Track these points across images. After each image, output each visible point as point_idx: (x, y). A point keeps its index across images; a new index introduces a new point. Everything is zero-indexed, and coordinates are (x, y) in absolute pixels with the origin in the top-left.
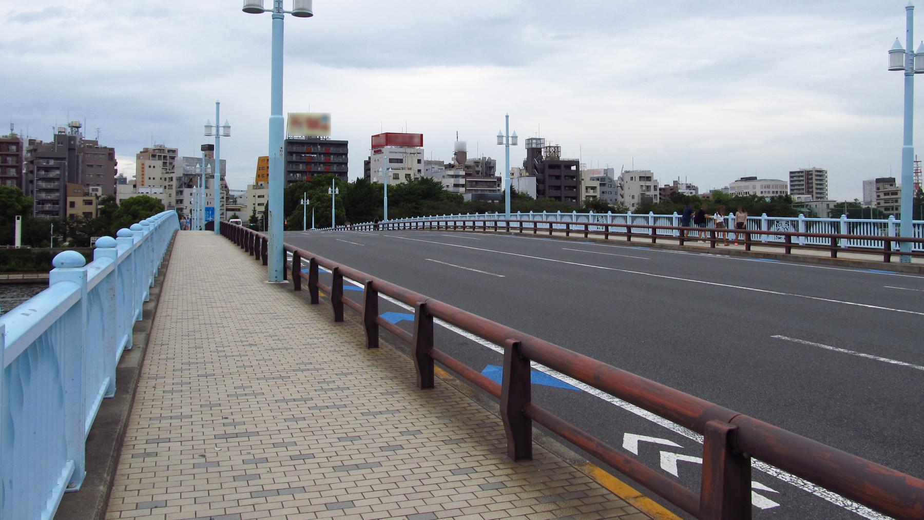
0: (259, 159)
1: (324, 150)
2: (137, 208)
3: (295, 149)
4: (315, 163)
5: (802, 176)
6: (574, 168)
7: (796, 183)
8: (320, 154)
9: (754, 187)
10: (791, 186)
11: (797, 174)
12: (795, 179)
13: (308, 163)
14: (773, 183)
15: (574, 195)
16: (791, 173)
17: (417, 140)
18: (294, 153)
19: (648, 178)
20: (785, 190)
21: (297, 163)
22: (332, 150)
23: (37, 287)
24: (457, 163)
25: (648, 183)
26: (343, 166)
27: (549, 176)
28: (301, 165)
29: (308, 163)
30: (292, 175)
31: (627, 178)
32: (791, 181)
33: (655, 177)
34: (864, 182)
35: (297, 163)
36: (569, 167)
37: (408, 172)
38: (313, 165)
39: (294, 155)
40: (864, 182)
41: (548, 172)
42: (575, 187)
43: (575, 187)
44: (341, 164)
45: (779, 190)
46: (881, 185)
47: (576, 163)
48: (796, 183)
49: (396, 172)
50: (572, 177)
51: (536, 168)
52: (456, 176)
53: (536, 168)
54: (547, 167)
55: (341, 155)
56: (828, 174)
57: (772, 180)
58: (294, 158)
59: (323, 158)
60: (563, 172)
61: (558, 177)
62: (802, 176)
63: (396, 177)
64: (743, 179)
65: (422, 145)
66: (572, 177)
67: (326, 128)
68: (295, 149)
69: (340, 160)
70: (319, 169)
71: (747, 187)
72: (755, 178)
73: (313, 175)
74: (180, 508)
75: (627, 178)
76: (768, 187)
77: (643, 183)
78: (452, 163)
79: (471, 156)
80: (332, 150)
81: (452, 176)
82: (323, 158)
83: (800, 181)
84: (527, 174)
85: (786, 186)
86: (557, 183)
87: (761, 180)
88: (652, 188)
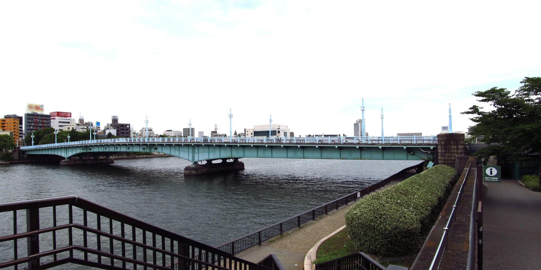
0: (126, 125)
1: (42, 118)
2: (5, 139)
3: (30, 117)
4: (38, 123)
5: (187, 130)
6: (128, 126)
7: (185, 132)
8: (40, 119)
9: (172, 133)
10: (184, 133)
11: (185, 129)
12: (185, 131)
13: (35, 123)
14: (178, 132)
15: (128, 136)
16: (184, 129)
17: (69, 115)
18: (30, 119)
19: (151, 130)
20: (181, 134)
21: (31, 122)
22: (45, 118)
23: (97, 173)
24: (80, 124)
25: (151, 132)
26: (49, 124)
27: (121, 129)
28: (33, 123)
29: (35, 123)
30: (29, 127)
31: (144, 130)
32: (184, 132)
33: (153, 130)
34: (199, 132)
35: (31, 122)
36: (126, 126)
37: (73, 127)
38: (37, 123)
39: (30, 120)
40: (199, 132)
41: (120, 128)
42: (128, 133)
43: (128, 133)
44: (48, 123)
45: (179, 135)
46: (213, 133)
47: (129, 125)
48: (185, 132)
49: (69, 127)
50: (128, 130)
51: (116, 126)
52: (83, 128)
53: (116, 126)
54: (120, 126)
55: (48, 120)
56: (195, 130)
57: (177, 131)
58: (30, 121)
59: (41, 121)
60: (125, 128)
61: (123, 130)
62: (187, 130)
63: (69, 128)
64: (167, 131)
65: (71, 117)
66: (128, 130)
67: (42, 110)
68: (30, 117)
69: (48, 122)
70: (40, 125)
71: (169, 133)
72: (171, 131)
73: (37, 127)
74: (57, 243)
75: (144, 130)
76: (176, 133)
77: (149, 132)
78: (78, 123)
79: (86, 121)
80: (45, 118)
81: (82, 128)
82: (41, 121)
83: (186, 132)
84: (113, 128)
85: (182, 133)
86: (123, 131)
87: (173, 131)
88: (152, 134)
